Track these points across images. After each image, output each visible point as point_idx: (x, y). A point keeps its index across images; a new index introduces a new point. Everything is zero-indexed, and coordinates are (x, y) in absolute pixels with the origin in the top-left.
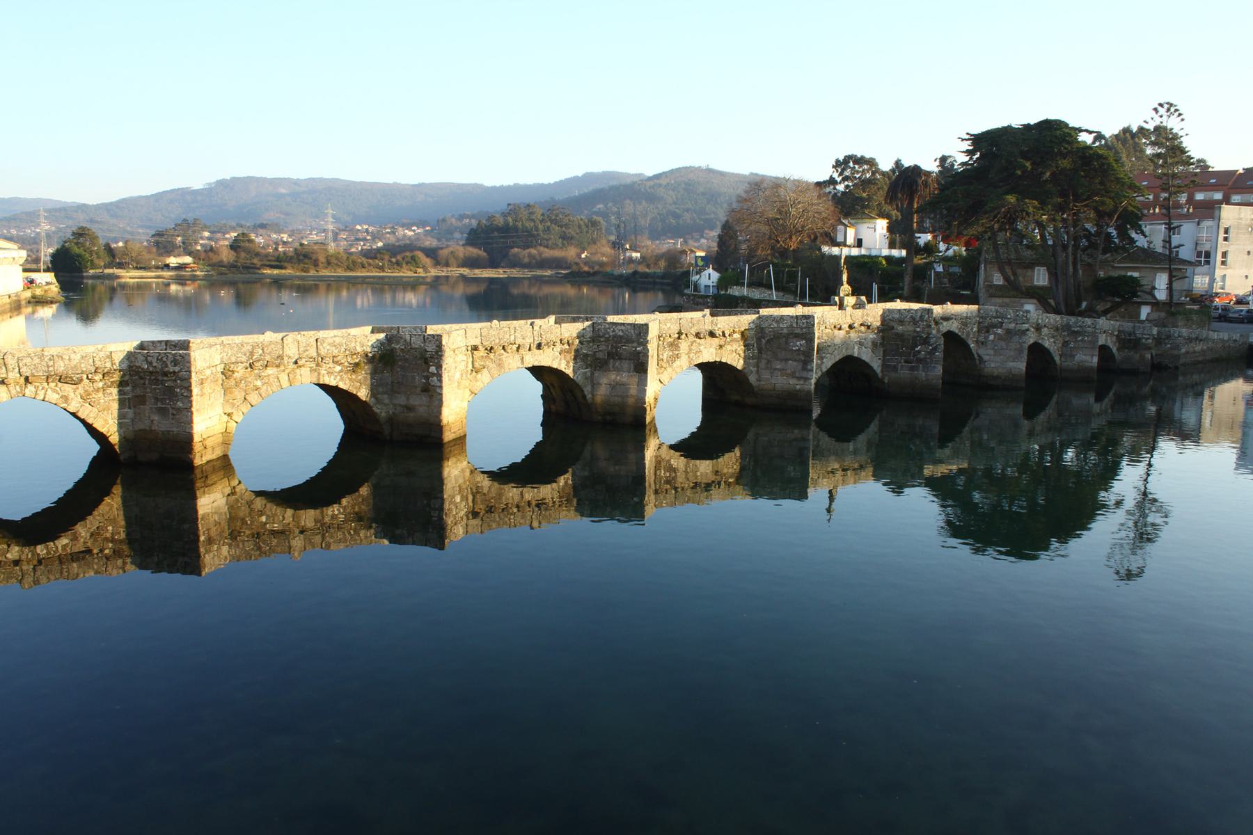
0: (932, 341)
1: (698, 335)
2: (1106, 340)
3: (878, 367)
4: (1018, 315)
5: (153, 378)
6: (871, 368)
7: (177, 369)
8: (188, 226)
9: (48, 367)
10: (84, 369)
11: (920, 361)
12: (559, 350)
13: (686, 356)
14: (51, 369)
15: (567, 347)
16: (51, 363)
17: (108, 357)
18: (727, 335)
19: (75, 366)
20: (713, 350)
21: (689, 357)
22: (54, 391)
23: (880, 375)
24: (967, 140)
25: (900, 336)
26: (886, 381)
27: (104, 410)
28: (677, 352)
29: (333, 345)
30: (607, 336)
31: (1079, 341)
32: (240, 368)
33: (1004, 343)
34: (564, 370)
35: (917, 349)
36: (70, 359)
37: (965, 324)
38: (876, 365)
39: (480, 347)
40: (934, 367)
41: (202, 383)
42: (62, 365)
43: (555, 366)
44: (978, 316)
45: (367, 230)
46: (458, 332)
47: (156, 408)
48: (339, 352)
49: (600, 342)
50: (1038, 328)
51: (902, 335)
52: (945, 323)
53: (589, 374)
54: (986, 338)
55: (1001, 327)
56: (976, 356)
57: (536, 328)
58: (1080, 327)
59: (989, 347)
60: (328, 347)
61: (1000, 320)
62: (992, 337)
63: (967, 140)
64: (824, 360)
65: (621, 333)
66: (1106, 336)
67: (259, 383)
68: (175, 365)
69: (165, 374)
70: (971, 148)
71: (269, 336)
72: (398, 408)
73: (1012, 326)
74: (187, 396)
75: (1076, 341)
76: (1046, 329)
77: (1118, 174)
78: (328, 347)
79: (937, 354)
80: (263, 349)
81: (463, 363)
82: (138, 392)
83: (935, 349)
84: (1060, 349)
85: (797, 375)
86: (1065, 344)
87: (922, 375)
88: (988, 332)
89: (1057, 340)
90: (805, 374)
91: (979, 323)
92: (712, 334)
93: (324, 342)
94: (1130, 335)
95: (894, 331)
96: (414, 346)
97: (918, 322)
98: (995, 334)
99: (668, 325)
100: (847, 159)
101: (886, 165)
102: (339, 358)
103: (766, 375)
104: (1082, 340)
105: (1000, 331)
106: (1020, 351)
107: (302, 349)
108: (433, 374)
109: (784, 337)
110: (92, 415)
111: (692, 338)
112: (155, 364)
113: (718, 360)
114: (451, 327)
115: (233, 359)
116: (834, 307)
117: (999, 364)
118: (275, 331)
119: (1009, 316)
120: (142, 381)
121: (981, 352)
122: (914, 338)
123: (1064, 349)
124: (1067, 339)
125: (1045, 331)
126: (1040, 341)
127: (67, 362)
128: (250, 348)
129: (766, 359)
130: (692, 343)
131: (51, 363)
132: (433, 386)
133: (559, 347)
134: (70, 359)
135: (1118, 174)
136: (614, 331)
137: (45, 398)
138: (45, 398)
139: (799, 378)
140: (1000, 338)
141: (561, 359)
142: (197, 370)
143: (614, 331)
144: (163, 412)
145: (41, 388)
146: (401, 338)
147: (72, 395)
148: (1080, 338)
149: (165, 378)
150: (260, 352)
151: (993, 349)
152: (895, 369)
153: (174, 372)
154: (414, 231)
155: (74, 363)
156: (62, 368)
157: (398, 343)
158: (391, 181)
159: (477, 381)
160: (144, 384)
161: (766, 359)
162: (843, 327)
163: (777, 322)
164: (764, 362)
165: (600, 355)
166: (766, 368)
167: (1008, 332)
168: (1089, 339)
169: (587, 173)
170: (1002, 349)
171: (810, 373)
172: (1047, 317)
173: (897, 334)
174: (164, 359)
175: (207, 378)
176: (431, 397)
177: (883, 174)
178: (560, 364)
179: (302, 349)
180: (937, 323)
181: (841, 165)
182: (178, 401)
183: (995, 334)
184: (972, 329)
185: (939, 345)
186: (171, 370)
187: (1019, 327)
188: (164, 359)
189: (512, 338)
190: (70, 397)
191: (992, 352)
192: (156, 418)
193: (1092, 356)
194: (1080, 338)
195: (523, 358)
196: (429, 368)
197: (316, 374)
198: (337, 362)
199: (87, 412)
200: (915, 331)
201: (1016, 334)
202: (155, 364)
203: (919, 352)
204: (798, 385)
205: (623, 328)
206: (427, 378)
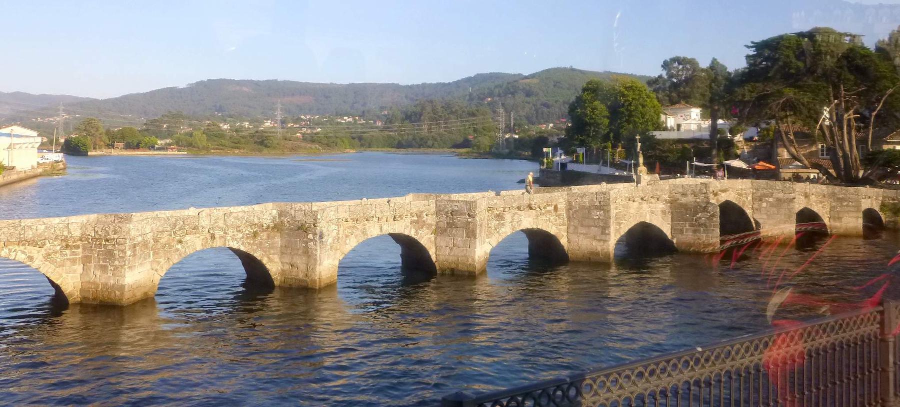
0: (710, 209)
1: (519, 208)
2: (872, 204)
3: (668, 230)
4: (785, 187)
5: (98, 243)
6: (662, 232)
7: (116, 237)
8: (176, 117)
9: (20, 235)
10: (47, 237)
11: (700, 225)
12: (410, 221)
13: (510, 225)
14: (22, 236)
15: (416, 219)
16: (22, 232)
17: (66, 227)
18: (542, 208)
19: (40, 234)
20: (530, 219)
21: (512, 225)
22: (23, 252)
23: (670, 237)
24: (752, 47)
25: (685, 206)
26: (675, 241)
27: (60, 266)
28: (502, 222)
29: (237, 218)
30: (446, 210)
31: (844, 206)
32: (165, 235)
33: (775, 209)
34: (413, 236)
35: (697, 216)
36: (37, 229)
37: (740, 195)
38: (667, 230)
39: (349, 219)
40: (713, 230)
41: (135, 247)
42: (31, 233)
43: (406, 233)
44: (752, 188)
45: (309, 119)
46: (331, 208)
47: (99, 265)
48: (242, 223)
49: (442, 214)
50: (806, 196)
51: (686, 205)
52: (723, 194)
53: (433, 239)
54: (760, 205)
55: (772, 196)
56: (752, 220)
57: (392, 205)
58: (845, 194)
59: (762, 212)
60: (233, 220)
61: (770, 191)
62: (764, 205)
63: (752, 47)
64: (622, 226)
65: (456, 208)
66: (871, 201)
67: (179, 246)
68: (115, 234)
69: (107, 240)
70: (755, 53)
71: (193, 211)
72: (285, 265)
73: (781, 195)
74: (122, 257)
75: (842, 206)
76: (813, 196)
77: (880, 68)
78: (233, 220)
79: (714, 219)
80: (183, 222)
81: (335, 232)
82: (87, 253)
83: (713, 216)
84: (828, 213)
85: (598, 238)
86: (832, 208)
87: (704, 237)
88: (761, 200)
89: (825, 205)
90: (603, 237)
91: (753, 194)
92: (530, 207)
93: (230, 216)
94: (894, 199)
95: (679, 201)
96: (297, 219)
97: (697, 194)
98: (767, 202)
99: (495, 201)
100: (674, 60)
101: (704, 64)
102: (241, 228)
103: (574, 238)
104: (847, 205)
105: (771, 199)
106: (790, 217)
107: (213, 221)
108: (311, 240)
109: (587, 208)
110: (50, 270)
111: (514, 211)
112: (100, 233)
113: (535, 227)
114: (330, 204)
115: (161, 229)
116: (632, 184)
117: (496, 288)
118: (197, 206)
119: (778, 188)
120: (90, 246)
121: (757, 217)
122: (696, 207)
123: (832, 212)
124: (834, 204)
125: (813, 198)
126: (810, 207)
127: (34, 231)
128: (173, 220)
129: (574, 226)
130: (514, 214)
131: (22, 232)
132: (311, 249)
133: (409, 220)
134: (37, 229)
135: (880, 68)
136: (451, 207)
137: (15, 258)
138: (15, 258)
139: (600, 240)
140: (772, 205)
141: (411, 228)
142: (131, 237)
143: (451, 207)
144: (104, 268)
145: (13, 250)
146: (288, 213)
147: (35, 255)
148: (845, 204)
149: (107, 243)
150: (182, 223)
151: (766, 214)
152: (681, 232)
153: (114, 239)
154: (345, 120)
155: (39, 231)
156: (31, 236)
157: (285, 217)
158: (328, 82)
159: (346, 244)
160: (91, 247)
161: (574, 226)
162: (636, 199)
163: (582, 197)
164: (572, 228)
165: (441, 225)
166: (574, 233)
167: (778, 200)
168: (853, 204)
169: (478, 74)
170: (774, 214)
171: (608, 236)
172: (814, 187)
173: (681, 204)
174: (107, 229)
175: (139, 243)
176: (309, 257)
177: (703, 70)
178: (410, 231)
179: (213, 221)
180: (716, 194)
181: (666, 65)
182: (115, 260)
183: (767, 202)
184: (747, 198)
185: (716, 212)
186: (112, 238)
187: (787, 196)
188: (107, 229)
189: (374, 212)
190: (35, 257)
191: (765, 216)
192: (98, 273)
193: (857, 218)
194: (845, 204)
195: (381, 227)
196: (307, 235)
197: (223, 239)
198: (240, 230)
199: (46, 269)
200: (696, 202)
201: (785, 201)
202: (100, 233)
203: (700, 218)
204: (598, 246)
205: (457, 204)
206: (306, 243)
